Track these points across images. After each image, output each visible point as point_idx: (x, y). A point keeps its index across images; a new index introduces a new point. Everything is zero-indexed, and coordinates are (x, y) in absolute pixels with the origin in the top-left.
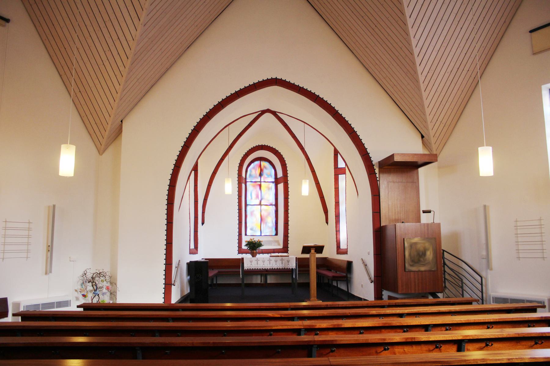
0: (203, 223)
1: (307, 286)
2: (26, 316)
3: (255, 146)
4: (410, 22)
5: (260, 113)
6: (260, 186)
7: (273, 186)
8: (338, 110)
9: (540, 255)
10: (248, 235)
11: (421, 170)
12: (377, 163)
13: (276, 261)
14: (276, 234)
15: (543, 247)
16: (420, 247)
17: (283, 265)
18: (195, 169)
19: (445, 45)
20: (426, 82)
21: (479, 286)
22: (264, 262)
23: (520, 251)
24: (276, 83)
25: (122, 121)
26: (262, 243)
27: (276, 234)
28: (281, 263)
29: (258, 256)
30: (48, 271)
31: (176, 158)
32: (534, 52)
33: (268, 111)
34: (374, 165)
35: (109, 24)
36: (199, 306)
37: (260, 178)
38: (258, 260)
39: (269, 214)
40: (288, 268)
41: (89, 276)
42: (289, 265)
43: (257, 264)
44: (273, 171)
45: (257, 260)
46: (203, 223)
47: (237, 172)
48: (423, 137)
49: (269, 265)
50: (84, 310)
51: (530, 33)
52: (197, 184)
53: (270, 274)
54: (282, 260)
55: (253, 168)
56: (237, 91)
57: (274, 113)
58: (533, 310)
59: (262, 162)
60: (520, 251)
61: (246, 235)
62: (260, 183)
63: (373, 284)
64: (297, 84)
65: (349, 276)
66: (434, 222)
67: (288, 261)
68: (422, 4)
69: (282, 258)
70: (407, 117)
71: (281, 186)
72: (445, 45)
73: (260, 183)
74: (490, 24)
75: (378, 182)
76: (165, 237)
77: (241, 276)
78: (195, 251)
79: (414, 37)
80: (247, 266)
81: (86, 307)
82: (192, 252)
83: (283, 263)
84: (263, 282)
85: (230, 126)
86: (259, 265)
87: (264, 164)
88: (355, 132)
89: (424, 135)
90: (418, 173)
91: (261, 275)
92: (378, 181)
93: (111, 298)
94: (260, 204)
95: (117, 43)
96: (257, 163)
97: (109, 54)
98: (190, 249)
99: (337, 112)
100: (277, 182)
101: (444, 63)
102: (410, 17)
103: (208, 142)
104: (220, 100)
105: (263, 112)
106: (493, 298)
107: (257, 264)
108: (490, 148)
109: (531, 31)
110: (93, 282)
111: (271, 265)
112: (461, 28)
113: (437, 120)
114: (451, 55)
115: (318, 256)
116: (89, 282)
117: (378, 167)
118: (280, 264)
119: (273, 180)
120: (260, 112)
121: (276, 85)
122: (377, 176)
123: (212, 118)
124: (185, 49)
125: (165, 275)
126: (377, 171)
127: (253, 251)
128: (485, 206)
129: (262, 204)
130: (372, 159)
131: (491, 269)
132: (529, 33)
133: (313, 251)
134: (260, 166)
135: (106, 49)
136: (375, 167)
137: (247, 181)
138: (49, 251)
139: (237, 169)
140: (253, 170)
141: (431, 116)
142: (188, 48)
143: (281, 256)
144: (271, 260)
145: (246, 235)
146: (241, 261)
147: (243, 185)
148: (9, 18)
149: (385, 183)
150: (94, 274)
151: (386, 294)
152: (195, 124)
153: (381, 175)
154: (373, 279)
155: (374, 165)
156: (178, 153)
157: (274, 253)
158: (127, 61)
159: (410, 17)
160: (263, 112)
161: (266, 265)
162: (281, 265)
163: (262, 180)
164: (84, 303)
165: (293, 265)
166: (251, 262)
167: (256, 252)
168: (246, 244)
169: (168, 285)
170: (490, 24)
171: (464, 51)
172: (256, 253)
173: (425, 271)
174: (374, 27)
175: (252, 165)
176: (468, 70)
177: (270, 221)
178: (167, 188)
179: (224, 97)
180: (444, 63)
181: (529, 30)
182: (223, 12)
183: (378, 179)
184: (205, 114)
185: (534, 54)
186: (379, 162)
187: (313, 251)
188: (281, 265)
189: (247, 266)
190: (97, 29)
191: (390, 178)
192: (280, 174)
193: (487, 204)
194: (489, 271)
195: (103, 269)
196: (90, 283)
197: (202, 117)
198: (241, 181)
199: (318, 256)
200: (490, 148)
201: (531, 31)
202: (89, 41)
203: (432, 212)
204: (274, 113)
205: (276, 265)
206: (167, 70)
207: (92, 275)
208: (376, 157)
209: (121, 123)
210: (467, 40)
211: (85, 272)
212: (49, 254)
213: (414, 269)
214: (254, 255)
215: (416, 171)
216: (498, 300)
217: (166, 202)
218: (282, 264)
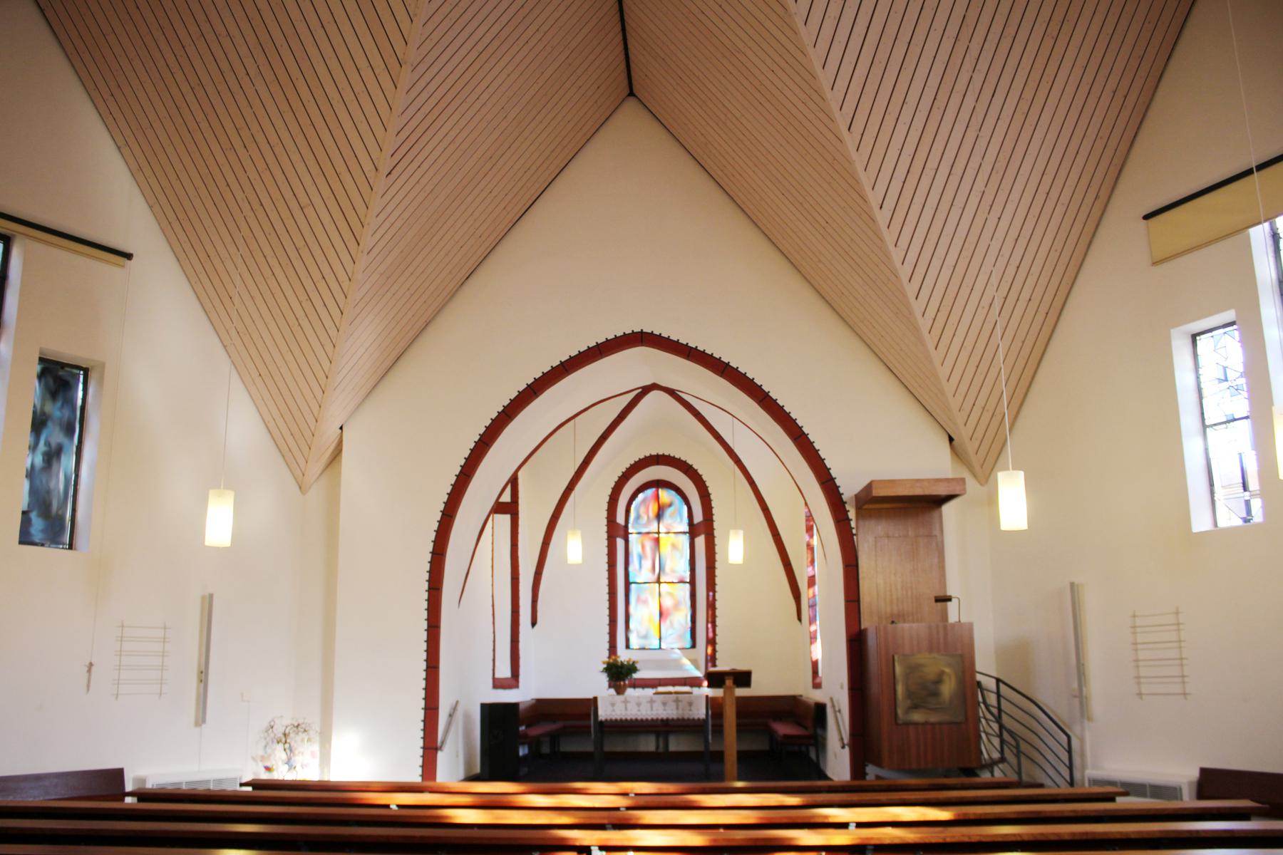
0: (534, 623)
1: (719, 756)
2: (143, 796)
3: (642, 457)
4: (882, 217)
5: (639, 393)
6: (657, 541)
7: (684, 541)
8: (769, 392)
9: (1178, 689)
10: (633, 649)
11: (947, 509)
12: (852, 498)
13: (664, 704)
14: (694, 646)
15: (1182, 671)
16: (931, 671)
17: (680, 712)
18: (509, 508)
19: (967, 253)
20: (936, 332)
21: (1065, 757)
22: (639, 705)
23: (1142, 680)
24: (642, 342)
25: (341, 428)
26: (638, 666)
27: (694, 646)
28: (624, 708)
29: (630, 692)
30: (201, 720)
31: (445, 498)
32: (1155, 261)
33: (654, 387)
34: (846, 503)
35: (305, 253)
36: (732, 837)
37: (655, 524)
38: (679, 701)
39: (677, 606)
40: (691, 717)
41: (279, 730)
42: (690, 713)
43: (626, 709)
44: (685, 508)
45: (626, 702)
46: (534, 623)
47: (605, 514)
48: (951, 439)
49: (649, 712)
50: (253, 789)
51: (1144, 221)
52: (517, 541)
53: (675, 732)
54: (677, 701)
55: (644, 501)
56: (601, 344)
57: (672, 392)
58: (1110, 798)
59: (660, 490)
60: (1142, 680)
61: (628, 647)
62: (656, 535)
63: (847, 750)
64: (683, 341)
65: (819, 731)
66: (960, 621)
67: (690, 704)
68: (903, 180)
69: (677, 698)
70: (916, 401)
71: (700, 541)
72: (967, 253)
73: (656, 535)
74: (1063, 204)
75: (855, 537)
76: (424, 656)
77: (593, 736)
78: (513, 682)
79: (896, 246)
80: (604, 713)
81: (257, 785)
82: (498, 684)
83: (654, 708)
84: (661, 749)
85: (577, 419)
86: (629, 712)
87: (666, 495)
88: (805, 436)
89: (953, 436)
90: (941, 516)
91: (658, 735)
92: (855, 535)
93: (322, 771)
94: (658, 581)
95: (321, 286)
96: (650, 492)
97: (307, 305)
98: (494, 678)
99: (766, 397)
100: (693, 531)
101: (972, 289)
102: (881, 208)
103: (523, 460)
104: (530, 381)
105: (646, 390)
106: (1089, 780)
107: (626, 709)
108: (1021, 474)
109: (1147, 217)
110: (286, 742)
111: (654, 712)
112: (999, 219)
113: (974, 405)
114: (1056, 251)
115: (741, 692)
116: (278, 743)
117: (854, 507)
118: (672, 710)
119: (687, 529)
120: (640, 390)
121: (642, 346)
122: (853, 524)
123: (515, 417)
124: (461, 282)
125: (424, 730)
126: (852, 514)
127: (622, 683)
128: (1072, 585)
129: (662, 580)
130: (841, 490)
131: (1090, 719)
132: (1142, 220)
133: (729, 682)
134: (657, 497)
135: (303, 297)
136: (848, 507)
137: (630, 531)
138: (201, 681)
139: (605, 506)
140: (643, 506)
141: (959, 397)
142: (467, 278)
143: (676, 693)
144: (655, 702)
145: (628, 647)
146: (590, 704)
147: (620, 543)
148: (131, 252)
149: (871, 539)
150: (287, 727)
151: (872, 771)
152: (482, 430)
153: (861, 523)
154: (846, 741)
155: (846, 503)
156: (449, 489)
157: (674, 685)
158: (341, 318)
159: (881, 208)
160: (646, 390)
161: (644, 712)
162: (675, 712)
163: (662, 529)
164: (253, 780)
165: (700, 712)
166: (613, 705)
167: (625, 684)
168: (604, 668)
169: (431, 748)
170: (1063, 204)
171: (1014, 262)
172: (625, 687)
173: (940, 724)
174: (823, 223)
175: (641, 496)
176: (1030, 300)
177: (681, 617)
178: (429, 557)
179: (539, 375)
180: (972, 289)
181: (1142, 216)
182: (532, 207)
183: (854, 531)
184: (501, 409)
185: (1154, 264)
186: (857, 497)
187: (729, 682)
188: (675, 712)
189: (604, 713)
190: (284, 260)
191: (880, 528)
192: (698, 517)
193: (1076, 581)
194: (1086, 722)
195: (304, 719)
196: (281, 745)
197: (494, 415)
198: (616, 531)
199: (741, 692)
200: (1021, 474)
201: (1147, 217)
202: (272, 282)
203: (953, 599)
204: (672, 392)
205: (664, 712)
206: (427, 324)
207: (284, 728)
208: (849, 488)
209: (340, 431)
210: (1017, 240)
211: (272, 724)
212: (202, 685)
213: (917, 717)
214: (620, 691)
215: (935, 514)
216: (1095, 782)
217: (426, 586)
218: (677, 708)
